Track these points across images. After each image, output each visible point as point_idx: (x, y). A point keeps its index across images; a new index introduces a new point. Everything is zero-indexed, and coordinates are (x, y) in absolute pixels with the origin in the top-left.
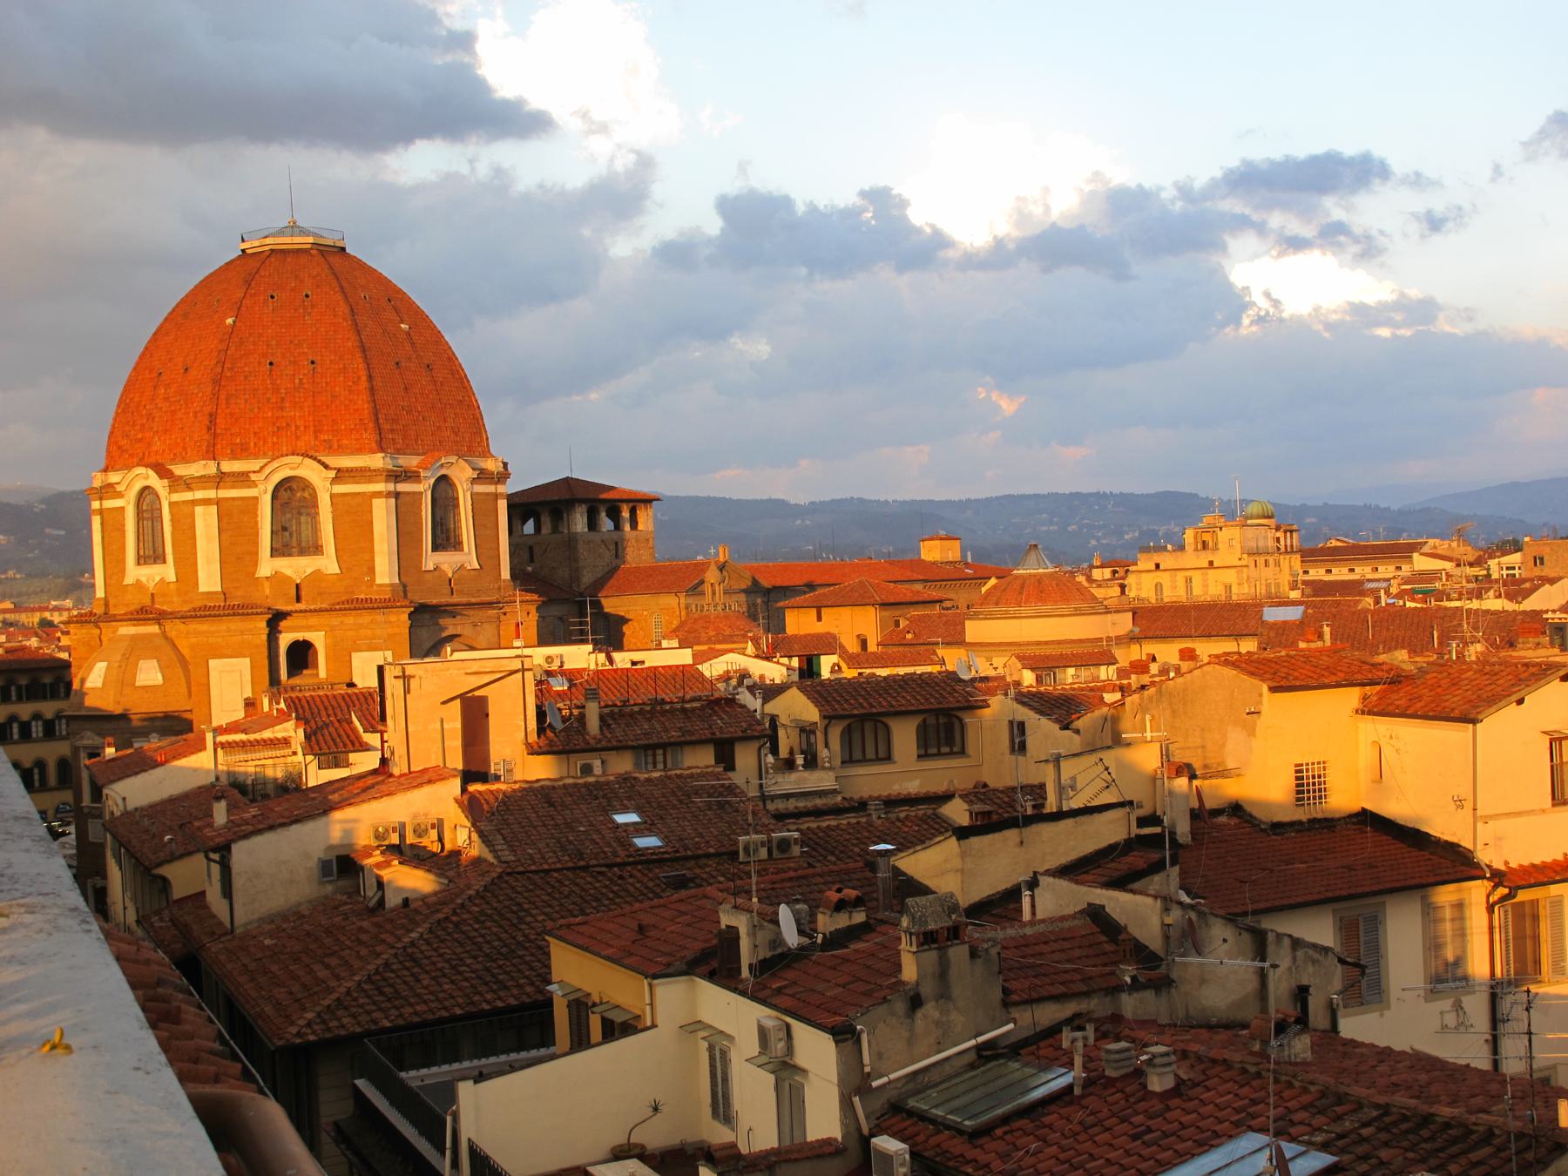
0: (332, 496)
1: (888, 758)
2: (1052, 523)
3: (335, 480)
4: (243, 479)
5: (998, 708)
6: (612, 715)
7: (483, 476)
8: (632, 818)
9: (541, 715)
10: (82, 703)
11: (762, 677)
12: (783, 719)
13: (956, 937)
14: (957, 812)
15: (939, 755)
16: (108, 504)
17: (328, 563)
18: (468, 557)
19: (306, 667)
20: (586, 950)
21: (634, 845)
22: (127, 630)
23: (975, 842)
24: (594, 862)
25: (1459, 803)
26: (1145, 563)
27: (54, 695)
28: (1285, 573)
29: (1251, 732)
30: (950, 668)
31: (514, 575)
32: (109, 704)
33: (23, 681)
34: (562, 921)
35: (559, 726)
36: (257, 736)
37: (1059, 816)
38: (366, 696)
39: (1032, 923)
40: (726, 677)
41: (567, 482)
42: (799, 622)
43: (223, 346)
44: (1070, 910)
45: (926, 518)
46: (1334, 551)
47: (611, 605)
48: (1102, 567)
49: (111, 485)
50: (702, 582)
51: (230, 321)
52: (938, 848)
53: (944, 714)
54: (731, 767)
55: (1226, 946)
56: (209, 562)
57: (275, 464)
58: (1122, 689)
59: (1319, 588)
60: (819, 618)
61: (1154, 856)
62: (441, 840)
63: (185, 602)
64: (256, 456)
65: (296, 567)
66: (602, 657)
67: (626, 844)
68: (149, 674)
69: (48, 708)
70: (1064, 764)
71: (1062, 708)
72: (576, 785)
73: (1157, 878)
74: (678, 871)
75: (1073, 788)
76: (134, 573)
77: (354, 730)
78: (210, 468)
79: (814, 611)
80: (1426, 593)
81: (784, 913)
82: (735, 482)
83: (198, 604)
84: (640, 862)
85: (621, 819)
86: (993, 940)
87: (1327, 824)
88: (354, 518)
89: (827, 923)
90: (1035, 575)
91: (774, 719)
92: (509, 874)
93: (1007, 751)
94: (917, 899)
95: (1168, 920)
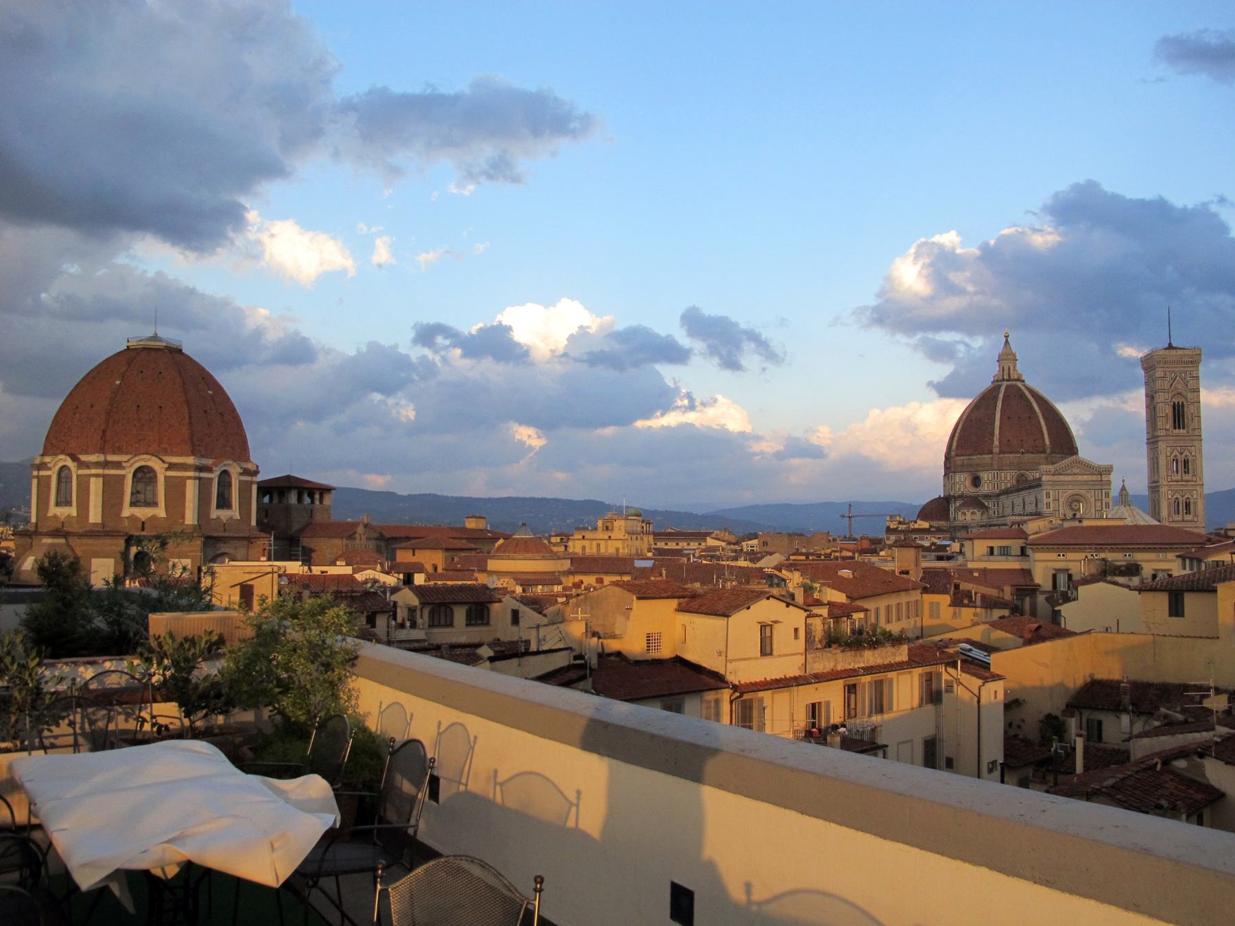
1: (451, 625)
3: (167, 469)
4: (118, 465)
7: (246, 472)
12: (400, 603)
14: (485, 652)
16: (43, 473)
17: (161, 512)
18: (234, 513)
23: (497, 663)
25: (720, 653)
26: (578, 536)
28: (645, 543)
29: (628, 618)
31: (259, 522)
37: (538, 653)
40: (366, 582)
41: (288, 478)
42: (403, 556)
46: (669, 534)
49: (45, 464)
53: (479, 606)
54: (374, 626)
56: (95, 507)
58: (566, 596)
59: (661, 552)
61: (581, 673)
65: (143, 513)
70: (541, 629)
71: (537, 604)
76: (54, 510)
78: (101, 458)
80: (712, 557)
82: (376, 482)
83: (87, 529)
87: (658, 662)
88: (176, 491)
91: (395, 603)
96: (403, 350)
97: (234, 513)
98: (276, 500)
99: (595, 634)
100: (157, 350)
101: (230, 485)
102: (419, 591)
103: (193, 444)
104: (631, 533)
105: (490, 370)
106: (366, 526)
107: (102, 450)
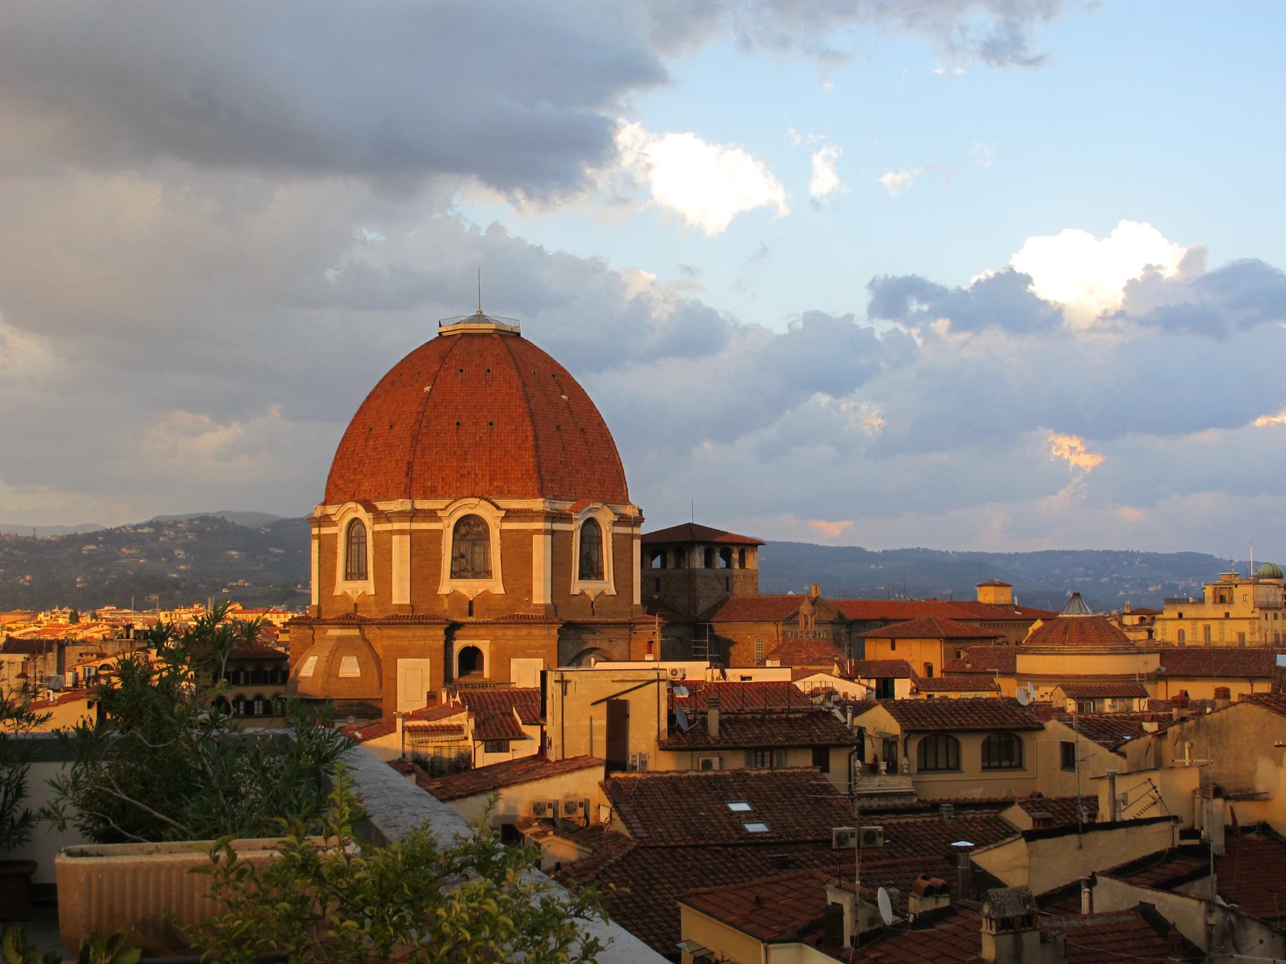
0: (501, 532)
1: (957, 768)
2: (1087, 575)
3: (505, 519)
4: (431, 515)
5: (1055, 730)
6: (729, 721)
7: (622, 520)
8: (744, 807)
9: (671, 717)
10: (296, 689)
11: (845, 694)
12: (869, 731)
13: (1029, 924)
15: (1000, 768)
16: (326, 531)
17: (495, 586)
18: (608, 585)
19: (474, 669)
20: (712, 915)
21: (745, 830)
22: (334, 632)
23: (1041, 843)
24: (712, 842)
26: (1170, 613)
27: (273, 681)
30: (1004, 694)
32: (317, 693)
33: (250, 669)
34: (692, 890)
35: (685, 727)
36: (437, 723)
37: (1113, 825)
38: (526, 694)
39: (1091, 915)
40: (814, 693)
41: (689, 526)
42: (877, 651)
43: (421, 409)
44: (1123, 907)
45: (981, 567)
47: (721, 629)
48: (1131, 614)
49: (328, 516)
50: (797, 613)
51: (427, 389)
52: (1008, 847)
53: (1007, 734)
54: (826, 769)
55: (1261, 947)
56: (401, 580)
57: (458, 504)
60: (893, 648)
61: (1196, 864)
62: (586, 816)
63: (381, 612)
64: (443, 497)
65: (470, 588)
66: (717, 672)
67: (740, 829)
68: (350, 668)
69: (268, 691)
70: (1117, 780)
72: (698, 777)
73: (1197, 883)
74: (782, 853)
75: (1125, 802)
76: (343, 587)
77: (515, 722)
79: (889, 642)
81: (882, 894)
82: (829, 533)
83: (391, 614)
84: (750, 845)
85: (735, 807)
86: (1060, 928)
88: (518, 549)
89: (916, 906)
90: (1077, 619)
91: (861, 730)
92: (642, 848)
93: (1059, 767)
94: (998, 890)
95: (1211, 921)
96: (862, 321)
98: (671, 565)
99: (1218, 792)
100: (484, 336)
102: (900, 710)
103: (541, 479)
104: (1264, 608)
105: (995, 344)
106: (814, 602)
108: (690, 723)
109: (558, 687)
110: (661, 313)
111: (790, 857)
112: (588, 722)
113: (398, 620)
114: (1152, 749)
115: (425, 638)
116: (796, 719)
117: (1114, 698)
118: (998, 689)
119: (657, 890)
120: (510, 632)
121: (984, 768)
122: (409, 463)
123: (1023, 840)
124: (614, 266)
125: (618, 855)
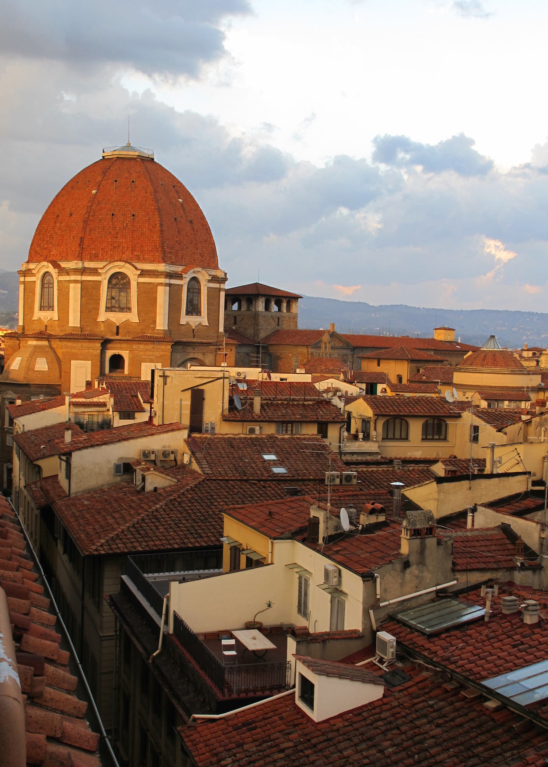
0: (138, 283)
1: (406, 439)
3: (141, 275)
4: (94, 271)
5: (468, 418)
6: (267, 404)
8: (273, 457)
9: (231, 401)
11: (346, 392)
12: (354, 414)
13: (431, 533)
14: (439, 469)
15: (433, 439)
16: (28, 279)
17: (133, 317)
18: (203, 319)
20: (242, 521)
21: (271, 471)
22: (33, 343)
23: (445, 485)
24: (251, 478)
31: (227, 329)
32: (20, 378)
35: (239, 406)
36: (91, 400)
37: (491, 476)
38: (145, 384)
40: (327, 391)
41: (256, 285)
43: (89, 204)
48: (528, 350)
49: (30, 270)
50: (320, 341)
51: (94, 192)
52: (426, 487)
54: (325, 436)
56: (74, 311)
57: (111, 265)
60: (379, 365)
61: (539, 501)
63: (62, 331)
64: (102, 260)
65: (118, 318)
66: (265, 375)
67: (269, 471)
68: (42, 364)
70: (496, 450)
74: (295, 487)
77: (139, 401)
82: (345, 293)
84: (275, 480)
85: (266, 457)
86: (450, 537)
89: (365, 520)
91: (349, 414)
92: (208, 480)
96: (369, 161)
97: (203, 319)
101: (199, 293)
103: (164, 252)
105: (449, 181)
107: (81, 257)
108: (243, 405)
109: (161, 379)
110: (248, 152)
111: (299, 488)
112: (179, 402)
113: (71, 337)
114: (522, 431)
115: (88, 348)
116: (309, 405)
117: (510, 401)
118: (439, 392)
119: (215, 506)
120: (142, 347)
121: (422, 439)
122: (81, 238)
123: (435, 483)
124: (221, 123)
125: (192, 484)
